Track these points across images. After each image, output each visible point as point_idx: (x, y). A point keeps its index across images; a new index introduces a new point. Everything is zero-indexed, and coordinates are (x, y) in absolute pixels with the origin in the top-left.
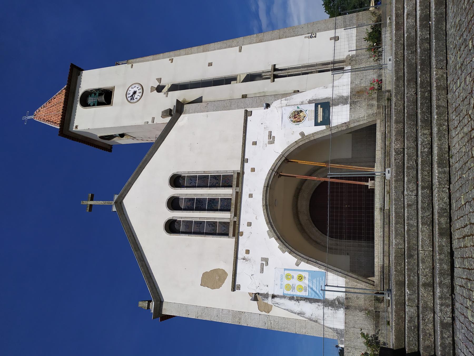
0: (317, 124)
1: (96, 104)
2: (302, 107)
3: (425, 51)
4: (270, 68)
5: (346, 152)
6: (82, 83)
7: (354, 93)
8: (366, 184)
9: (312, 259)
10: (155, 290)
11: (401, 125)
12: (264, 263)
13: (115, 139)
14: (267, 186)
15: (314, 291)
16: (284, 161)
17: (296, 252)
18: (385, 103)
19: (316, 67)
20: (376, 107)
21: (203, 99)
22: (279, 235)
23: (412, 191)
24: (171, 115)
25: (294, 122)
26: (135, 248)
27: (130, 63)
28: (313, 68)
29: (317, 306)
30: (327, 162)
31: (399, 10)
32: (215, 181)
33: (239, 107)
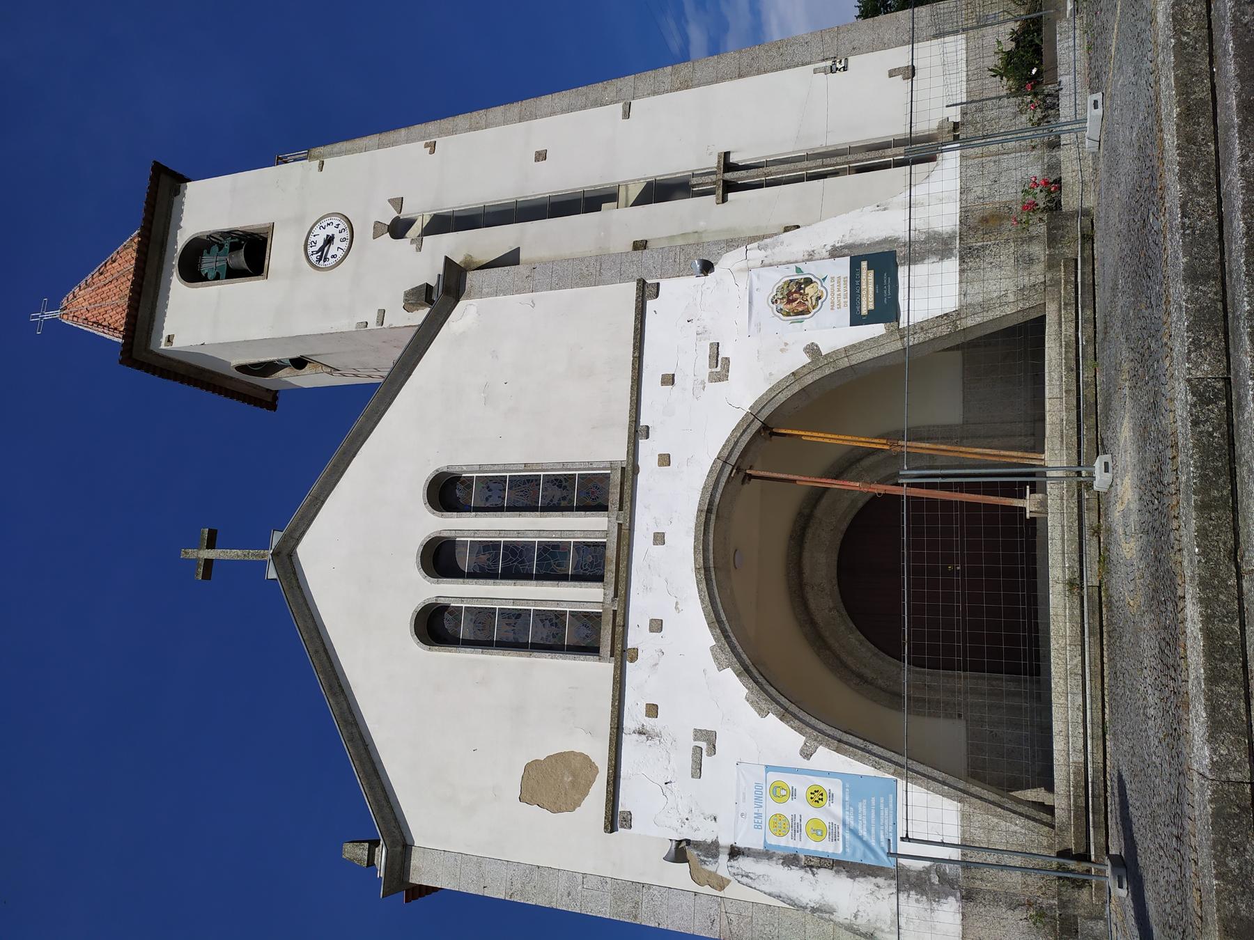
0: (857, 319)
1: (223, 274)
2: (810, 269)
4: (713, 162)
5: (944, 405)
6: (185, 216)
7: (971, 221)
8: (1017, 503)
9: (851, 739)
10: (387, 810)
11: (1210, 290)
12: (703, 745)
13: (281, 374)
14: (709, 511)
15: (861, 838)
16: (758, 432)
17: (802, 714)
18: (1074, 249)
19: (850, 158)
20: (1042, 266)
21: (522, 256)
22: (748, 662)
24: (429, 301)
25: (788, 314)
27: (317, 158)
28: (839, 159)
29: (872, 887)
30: (893, 436)
32: (558, 493)
33: (622, 277)
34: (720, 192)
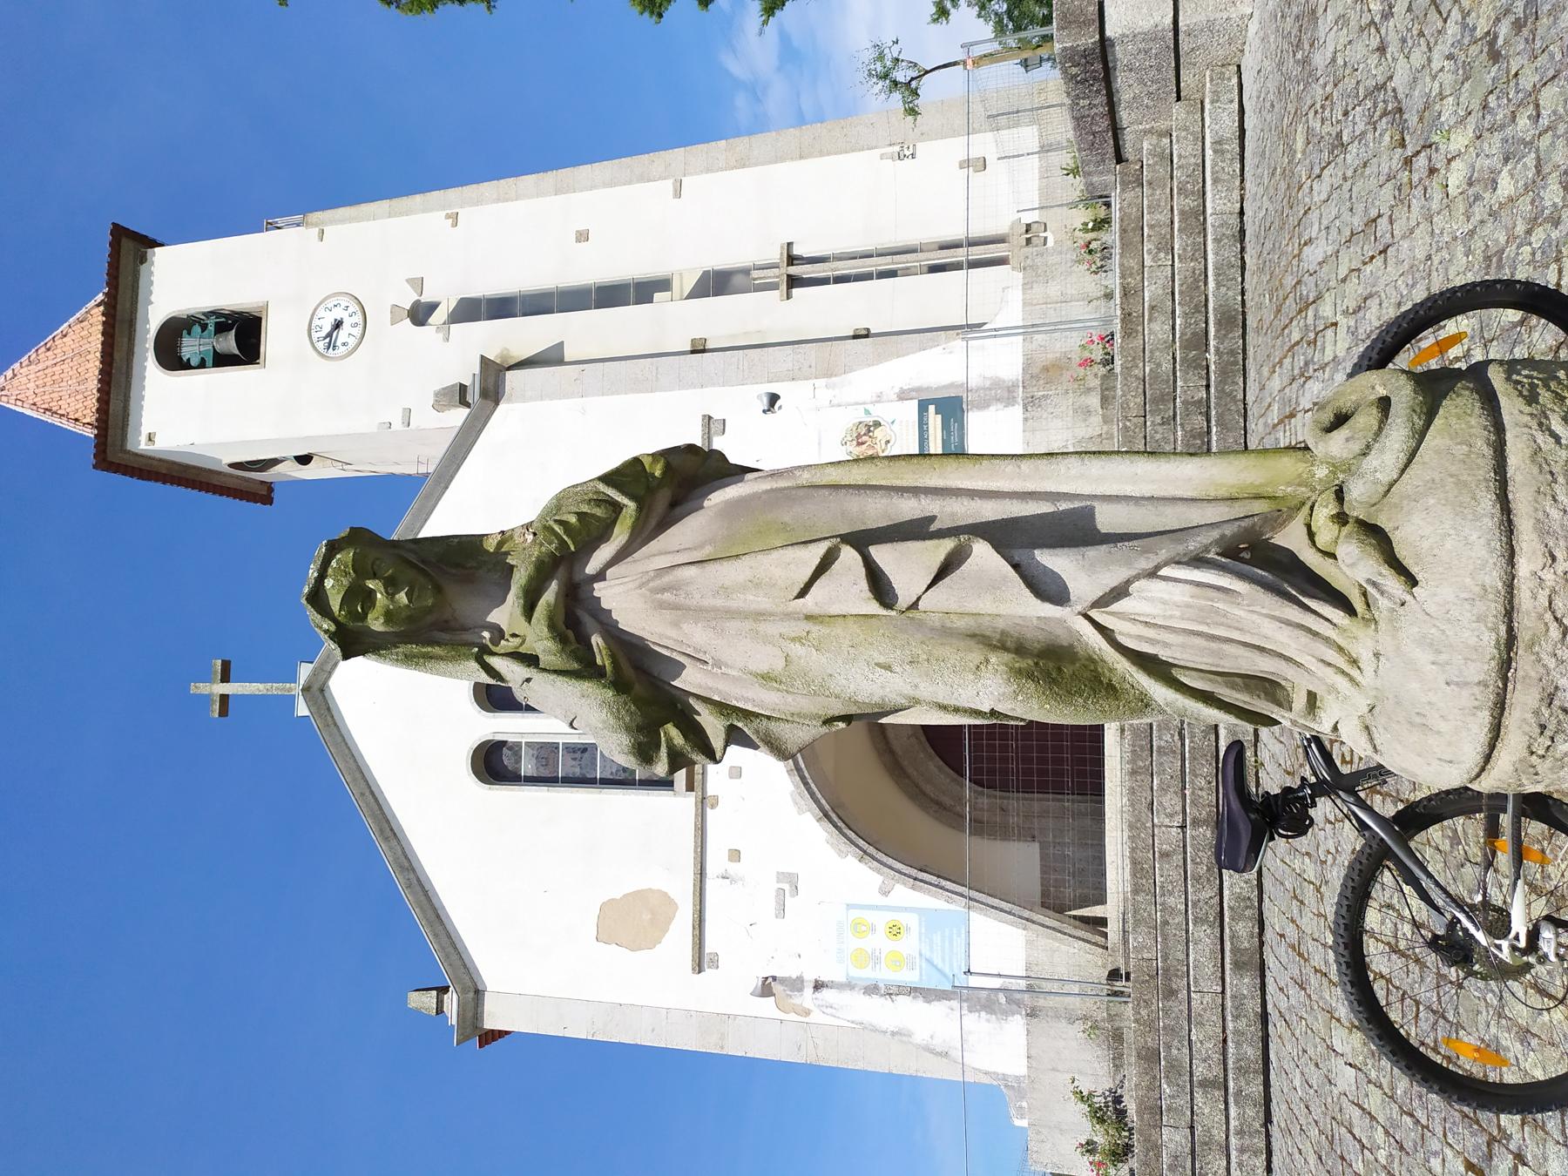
1: (209, 361)
2: (879, 412)
3: (1194, 437)
4: (775, 254)
6: (155, 288)
7: (1035, 371)
10: (454, 957)
12: (786, 887)
15: (935, 967)
19: (920, 256)
22: (827, 807)
23: (1171, 816)
24: (464, 402)
26: (382, 831)
27: (316, 225)
31: (1131, 275)
34: (784, 287)
